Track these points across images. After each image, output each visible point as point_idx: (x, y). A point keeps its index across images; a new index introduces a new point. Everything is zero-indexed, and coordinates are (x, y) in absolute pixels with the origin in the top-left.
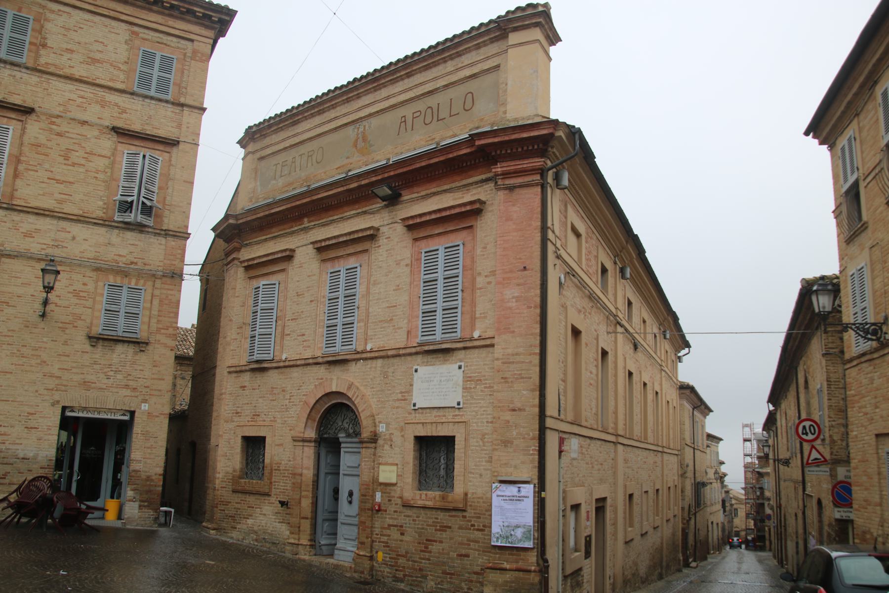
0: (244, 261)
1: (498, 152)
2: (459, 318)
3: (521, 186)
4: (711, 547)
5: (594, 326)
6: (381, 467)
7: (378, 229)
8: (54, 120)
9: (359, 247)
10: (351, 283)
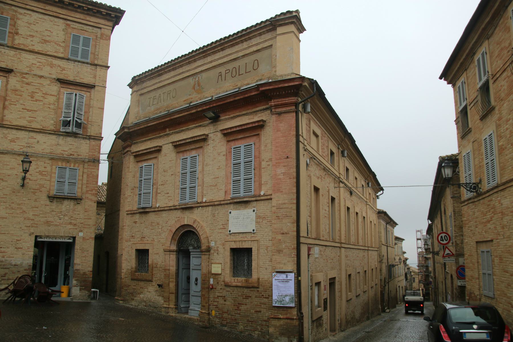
0: (134, 153)
1: (272, 94)
2: (253, 184)
3: (285, 112)
4: (399, 300)
5: (327, 186)
6: (213, 265)
7: (207, 135)
8: (24, 76)
9: (198, 145)
10: (194, 165)
